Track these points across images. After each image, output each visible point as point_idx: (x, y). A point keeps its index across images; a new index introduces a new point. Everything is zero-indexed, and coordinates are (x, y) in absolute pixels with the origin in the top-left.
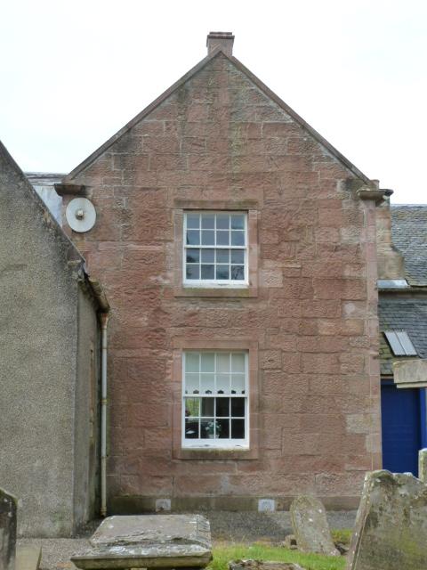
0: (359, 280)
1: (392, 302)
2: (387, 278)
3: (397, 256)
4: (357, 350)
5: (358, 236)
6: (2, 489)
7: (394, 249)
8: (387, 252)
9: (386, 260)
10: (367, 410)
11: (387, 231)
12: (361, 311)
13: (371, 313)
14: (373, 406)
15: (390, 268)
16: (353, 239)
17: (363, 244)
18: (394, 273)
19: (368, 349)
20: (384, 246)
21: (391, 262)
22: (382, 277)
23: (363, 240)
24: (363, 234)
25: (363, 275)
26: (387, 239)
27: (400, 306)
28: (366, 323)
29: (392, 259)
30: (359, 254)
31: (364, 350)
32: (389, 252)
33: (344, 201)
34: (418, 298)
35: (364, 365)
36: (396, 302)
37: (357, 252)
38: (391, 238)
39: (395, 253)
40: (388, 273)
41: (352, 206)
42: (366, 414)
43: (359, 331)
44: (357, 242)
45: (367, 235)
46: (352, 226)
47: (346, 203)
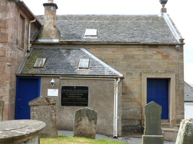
0: (5, 34)
1: (51, 48)
2: (51, 39)
3: (56, 30)
4: (2, 63)
5: (6, 16)
6: (179, 139)
7: (55, 27)
8: (51, 28)
9: (51, 32)
10: (4, 87)
11: (53, 20)
12: (5, 47)
13: (8, 48)
14: (6, 85)
15: (53, 35)
16: (4, 17)
17: (8, 20)
18: (54, 37)
19: (7, 62)
20: (51, 26)
21: (53, 32)
22: (49, 38)
23: (8, 18)
24: (8, 15)
25: (7, 32)
26: (52, 23)
27: (53, 50)
28: (6, 52)
29: (54, 31)
30: (6, 24)
31: (5, 63)
32: (53, 28)
33: (1, 2)
34: (63, 47)
35: (4, 68)
36: (53, 48)
37: (5, 23)
38: (54, 23)
39: (55, 29)
40: (52, 37)
41: (5, 4)
42: (3, 88)
43: (3, 55)
44: (5, 19)
45: (9, 16)
46: (4, 12)
47: (3, 3)
